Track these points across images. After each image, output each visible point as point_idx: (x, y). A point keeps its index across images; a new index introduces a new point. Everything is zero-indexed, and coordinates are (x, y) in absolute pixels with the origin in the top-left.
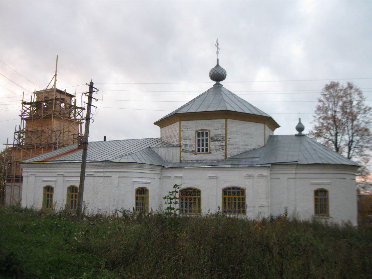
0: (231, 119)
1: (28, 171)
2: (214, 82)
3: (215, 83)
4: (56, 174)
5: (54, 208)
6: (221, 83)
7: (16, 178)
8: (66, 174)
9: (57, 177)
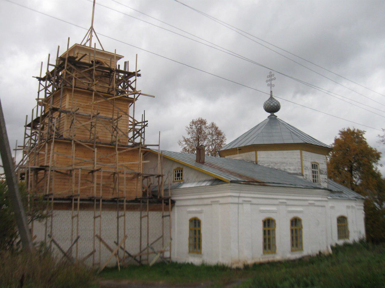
0: (261, 150)
1: (242, 195)
2: (269, 113)
3: (269, 114)
4: (276, 202)
5: (14, 239)
6: (275, 114)
7: (81, 202)
8: (289, 202)
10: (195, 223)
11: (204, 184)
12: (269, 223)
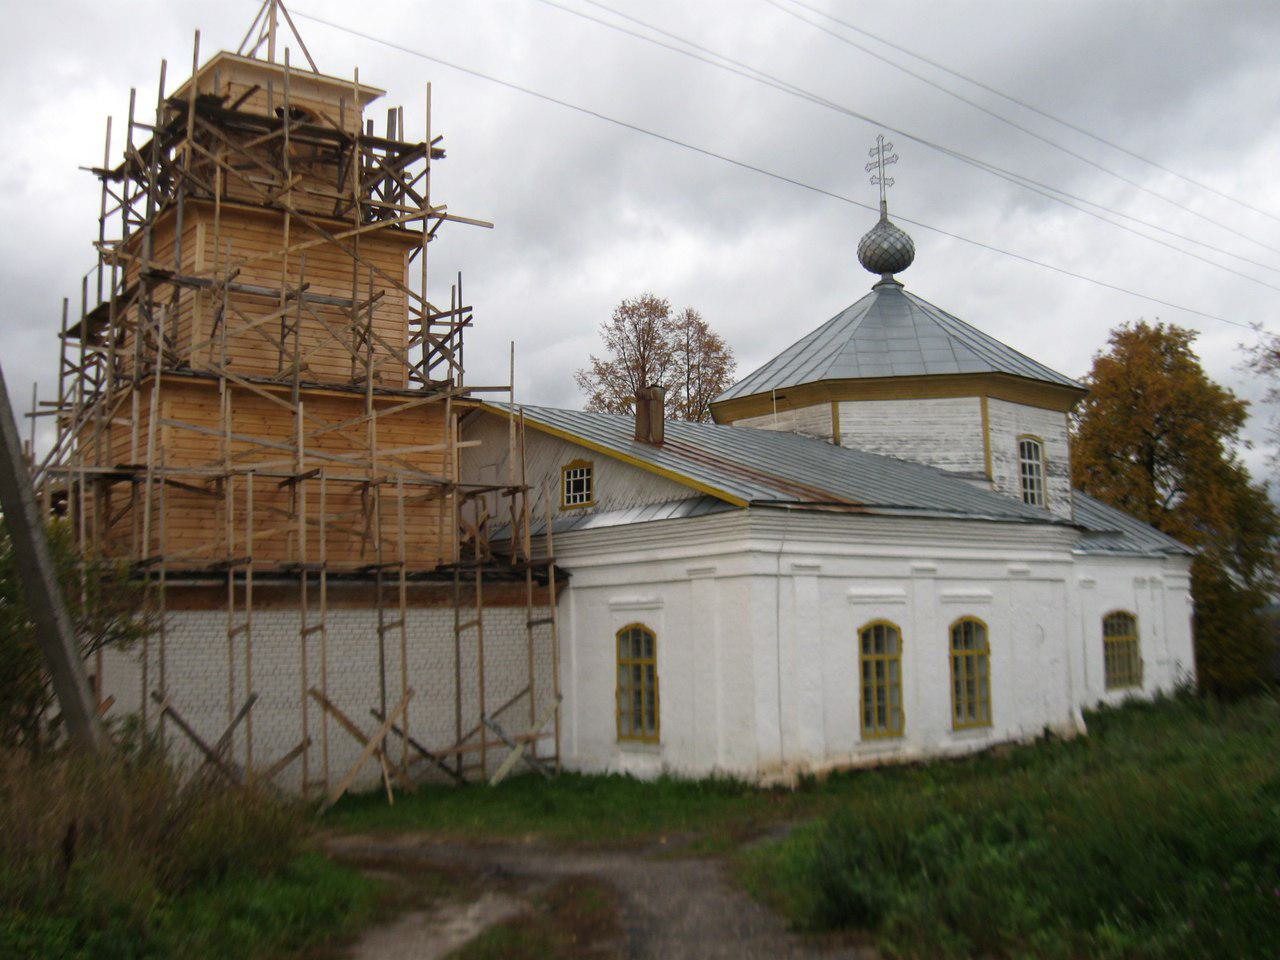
1: (787, 547)
3: (878, 278)
4: (904, 568)
6: (897, 277)
8: (944, 569)
9: (908, 582)
10: (638, 643)
11: (663, 514)
12: (878, 640)
